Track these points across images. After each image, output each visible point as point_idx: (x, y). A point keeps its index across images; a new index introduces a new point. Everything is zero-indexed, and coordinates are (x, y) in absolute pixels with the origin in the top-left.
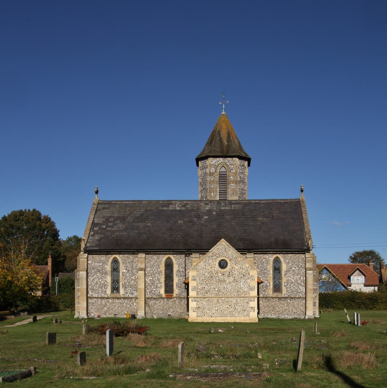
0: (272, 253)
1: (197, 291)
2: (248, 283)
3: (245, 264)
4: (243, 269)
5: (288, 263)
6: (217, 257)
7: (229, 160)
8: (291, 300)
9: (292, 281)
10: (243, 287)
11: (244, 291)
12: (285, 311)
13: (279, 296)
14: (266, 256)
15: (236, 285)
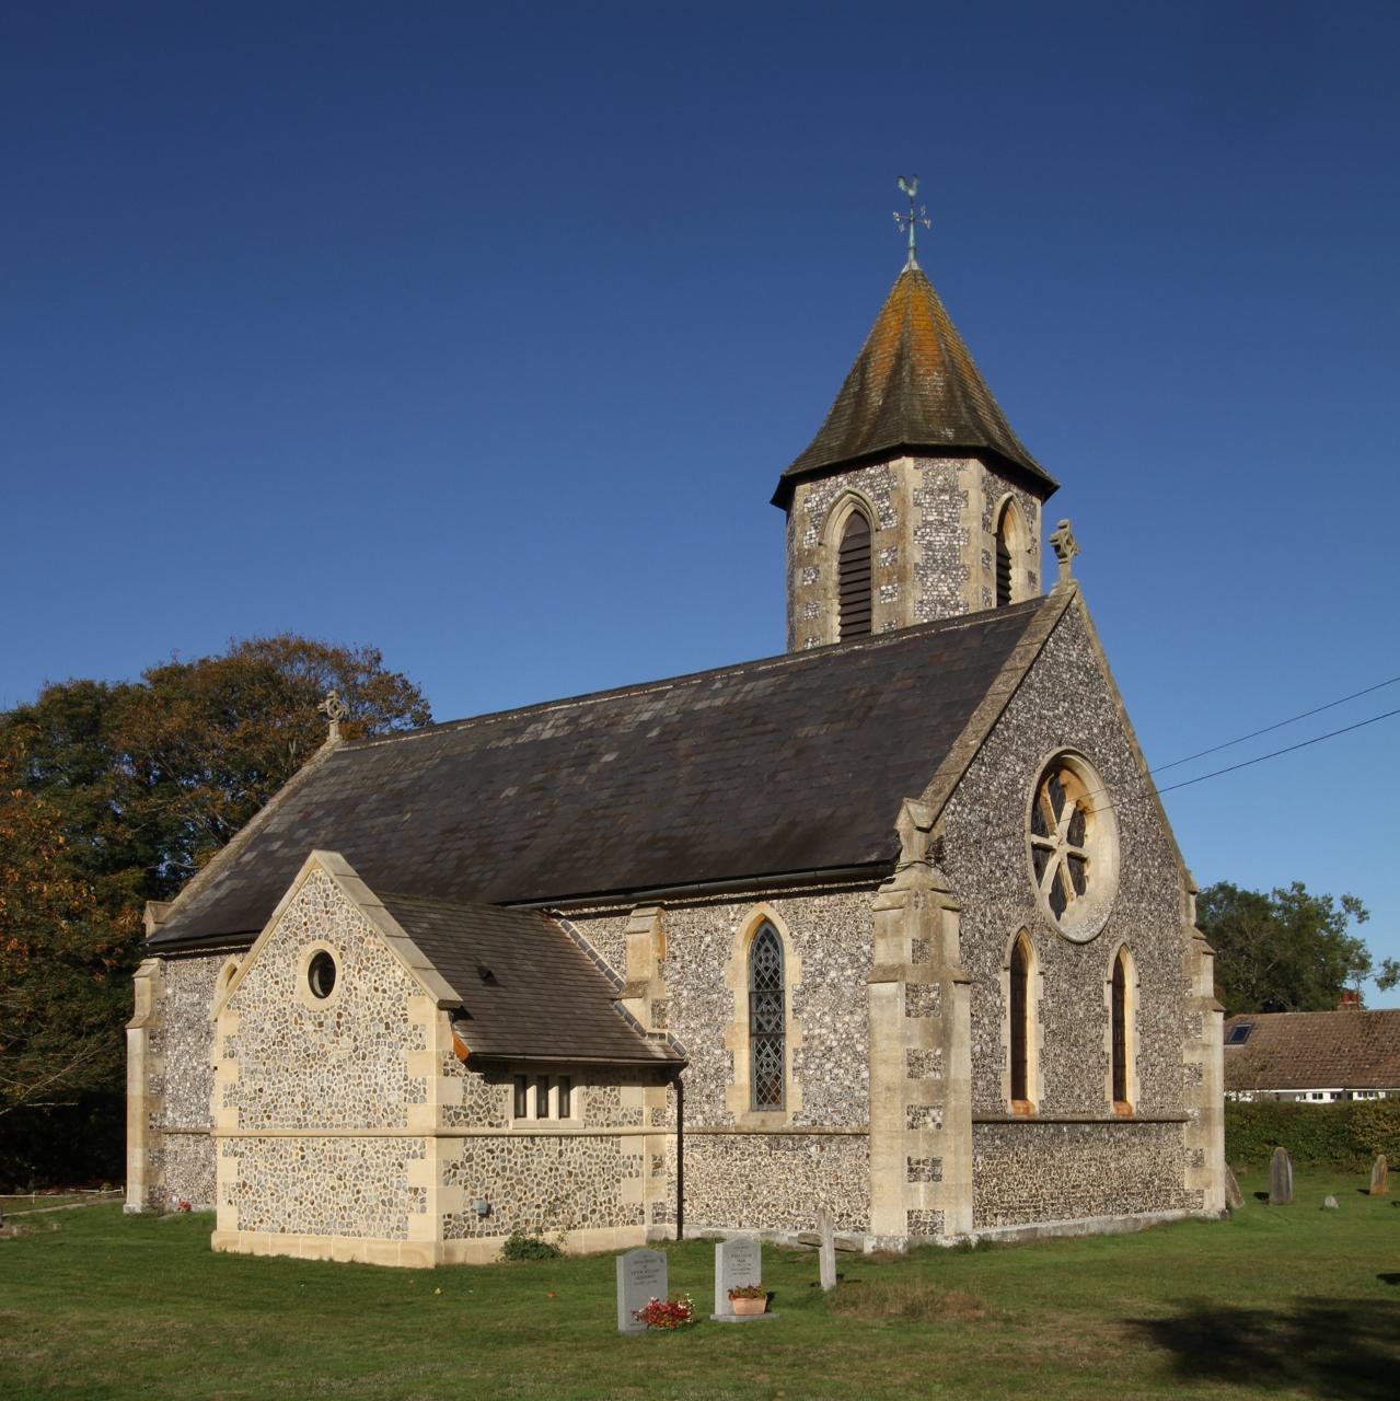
0: (775, 891)
1: (240, 1109)
2: (403, 1066)
3: (392, 967)
4: (384, 991)
5: (811, 944)
6: (302, 942)
7: (872, 477)
8: (822, 1149)
9: (828, 1043)
10: (386, 1086)
11: (389, 1104)
12: (798, 1205)
13: (773, 1126)
14: (717, 917)
15: (360, 1077)
